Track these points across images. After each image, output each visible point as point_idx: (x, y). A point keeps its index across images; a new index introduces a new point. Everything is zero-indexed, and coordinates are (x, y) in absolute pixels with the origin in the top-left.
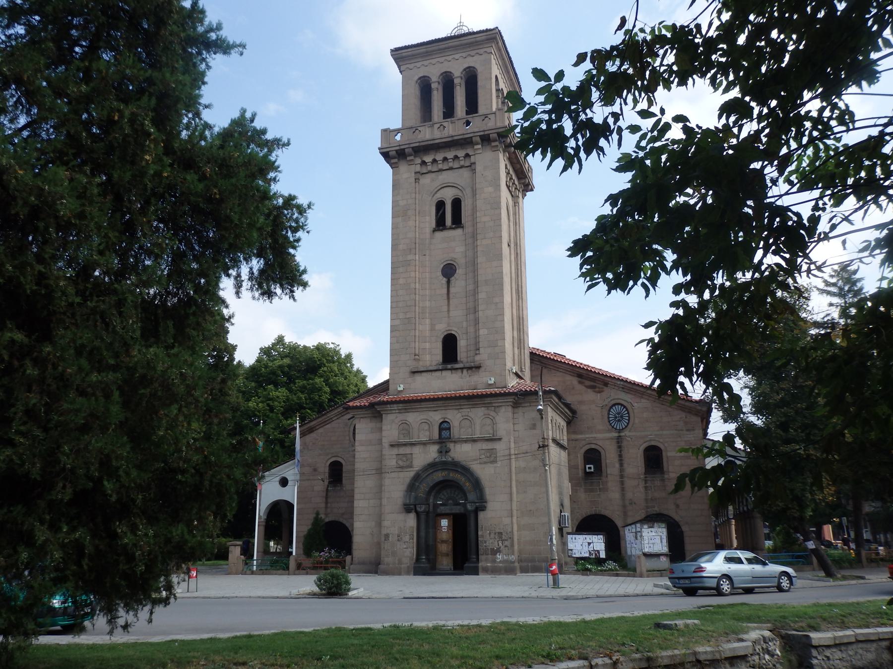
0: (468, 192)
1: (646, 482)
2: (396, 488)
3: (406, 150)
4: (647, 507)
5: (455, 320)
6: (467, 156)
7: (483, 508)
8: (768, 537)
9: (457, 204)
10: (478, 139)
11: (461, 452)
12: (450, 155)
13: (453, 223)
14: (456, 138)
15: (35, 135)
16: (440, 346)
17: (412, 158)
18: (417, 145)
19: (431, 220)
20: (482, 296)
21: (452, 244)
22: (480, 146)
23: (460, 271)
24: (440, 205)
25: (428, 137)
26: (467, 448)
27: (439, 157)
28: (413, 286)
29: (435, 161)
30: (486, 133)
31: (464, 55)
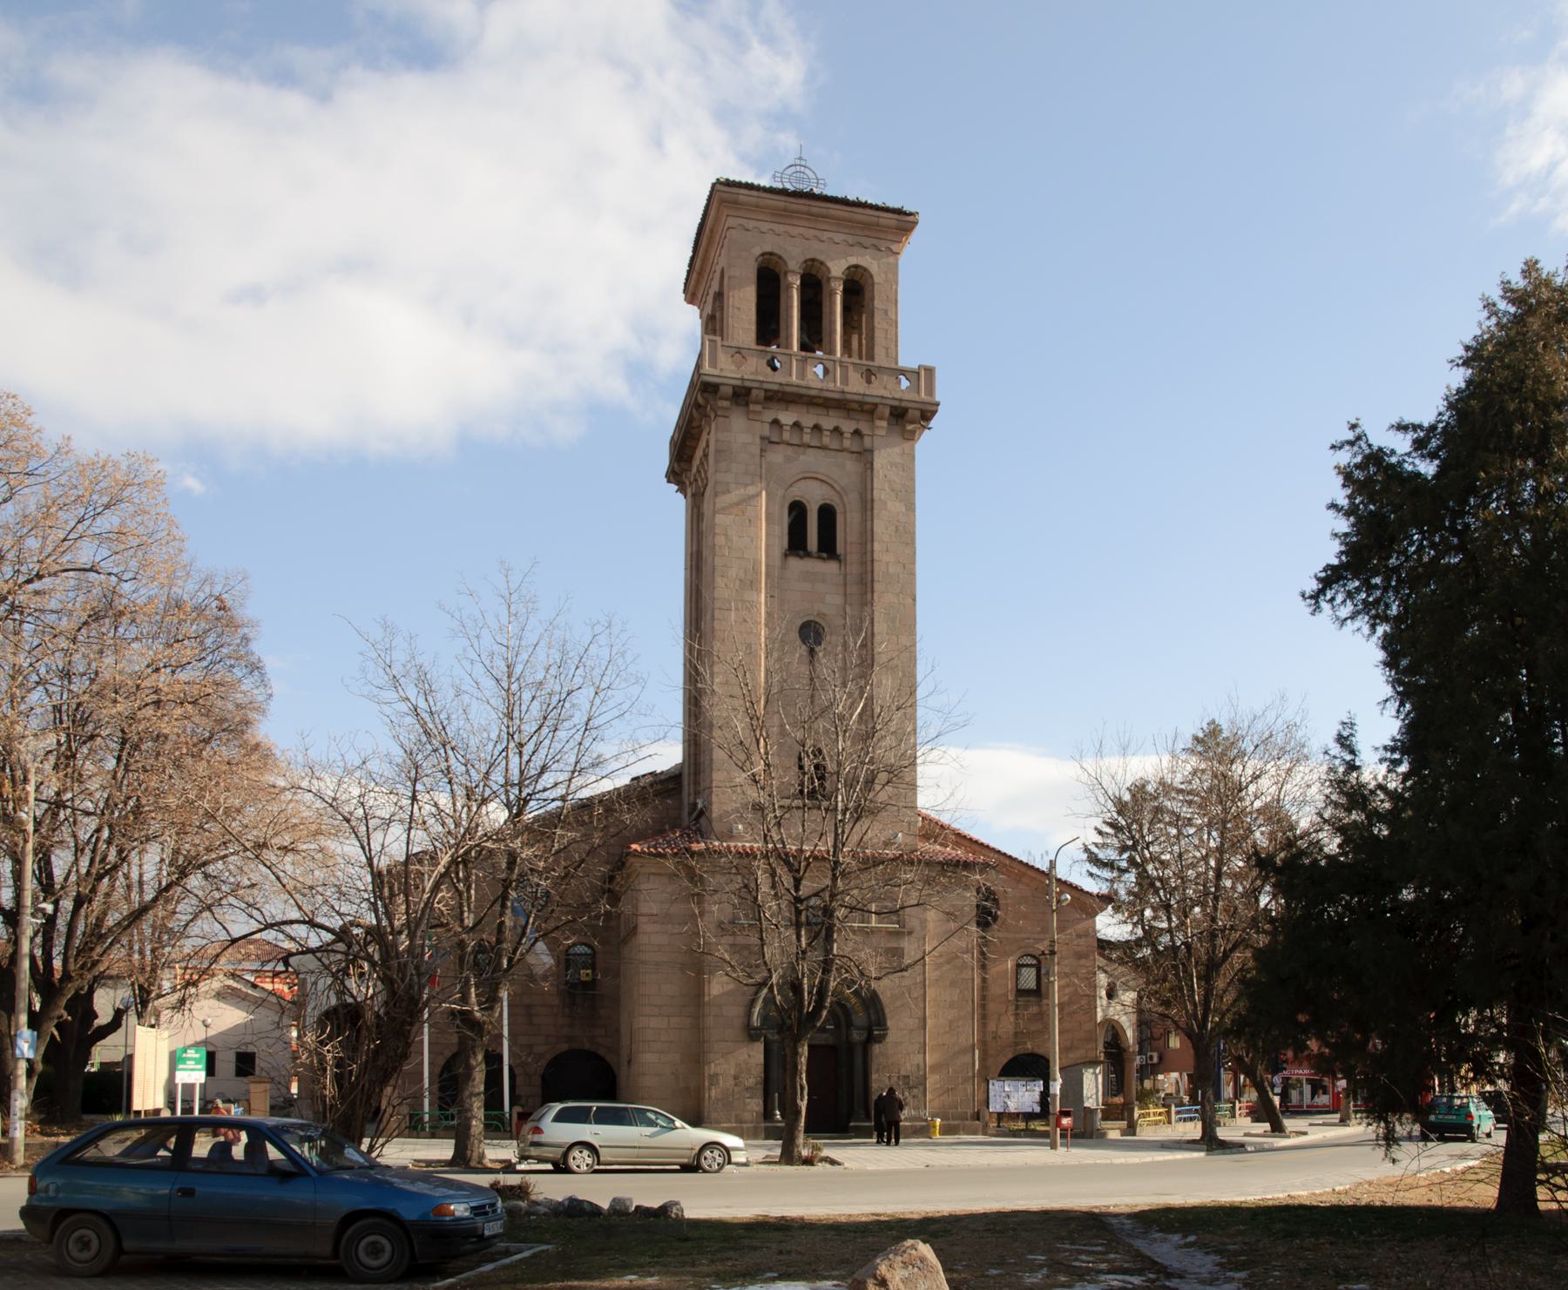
0: (852, 499)
3: (754, 392)
6: (857, 433)
7: (881, 1039)
8: (1360, 901)
9: (827, 515)
10: (887, 412)
12: (828, 422)
13: (820, 549)
15: (1420, 558)
17: (758, 408)
18: (775, 387)
22: (884, 424)
24: (797, 510)
30: (904, 404)
31: (851, 239)
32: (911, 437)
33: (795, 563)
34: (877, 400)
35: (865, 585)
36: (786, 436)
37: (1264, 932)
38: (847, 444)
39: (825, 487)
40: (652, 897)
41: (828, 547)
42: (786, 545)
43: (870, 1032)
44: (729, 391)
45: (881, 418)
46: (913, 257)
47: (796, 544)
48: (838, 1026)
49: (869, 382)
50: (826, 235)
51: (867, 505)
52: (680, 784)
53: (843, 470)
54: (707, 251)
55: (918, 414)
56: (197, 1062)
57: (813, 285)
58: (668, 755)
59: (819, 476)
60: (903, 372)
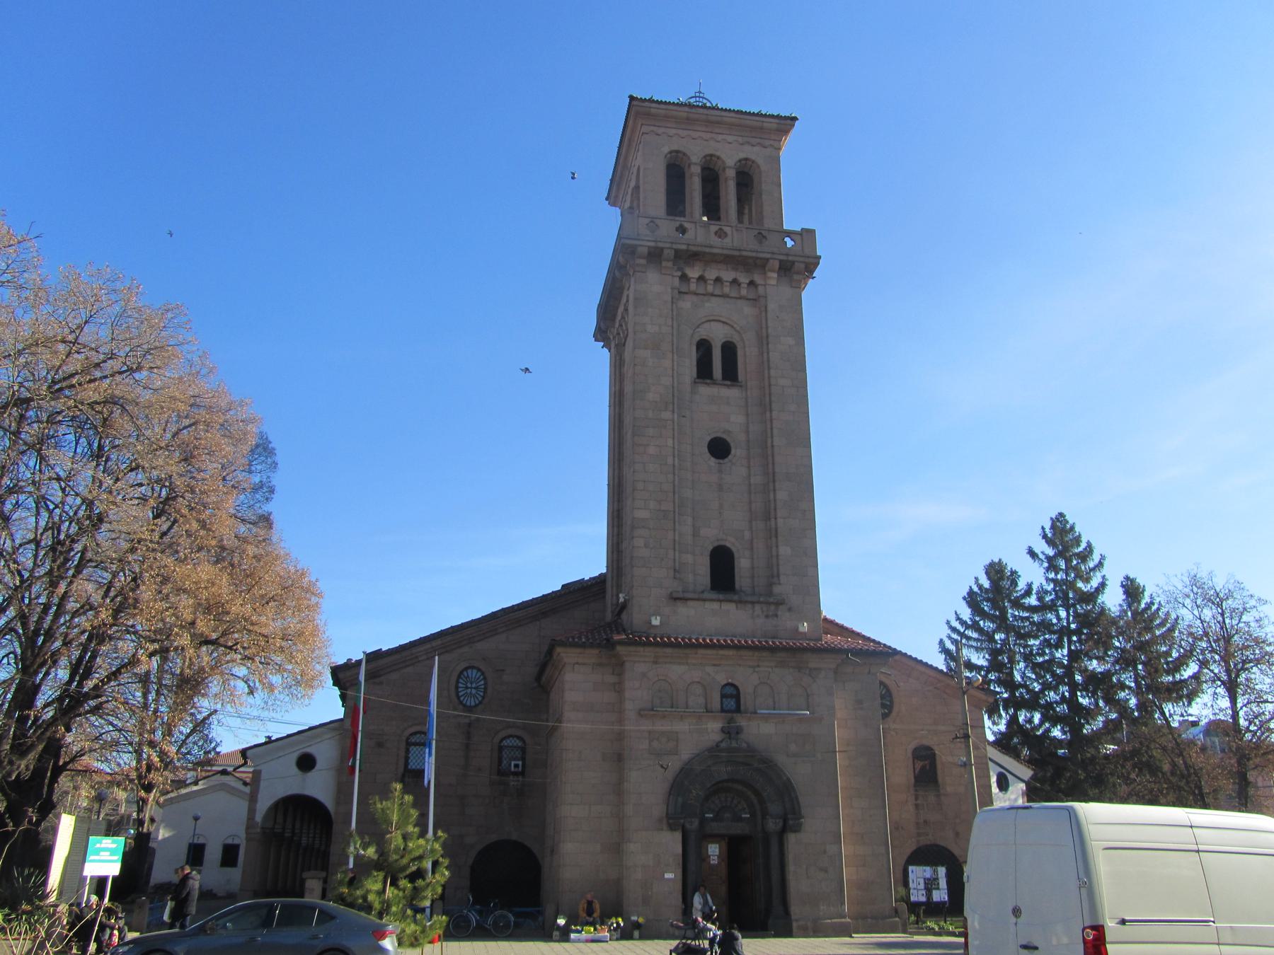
1: (916, 799)
2: (648, 786)
3: (666, 252)
4: (919, 835)
5: (729, 524)
7: (797, 829)
9: (729, 350)
10: (777, 265)
11: (760, 731)
12: (728, 275)
13: (724, 378)
14: (744, 253)
16: (706, 561)
18: (684, 247)
19: (689, 366)
20: (782, 495)
21: (722, 409)
22: (775, 275)
23: (737, 452)
24: (704, 347)
25: (700, 240)
26: (767, 729)
27: (711, 274)
28: (670, 461)
29: (701, 279)
32: (798, 287)
33: (705, 390)
34: (768, 256)
35: (765, 406)
36: (693, 286)
37: (1163, 713)
38: (744, 292)
39: (727, 327)
40: (578, 680)
41: (731, 374)
42: (695, 375)
43: (785, 821)
44: (645, 250)
45: (773, 271)
46: (791, 149)
47: (704, 371)
48: (753, 815)
49: (761, 242)
50: (720, 137)
51: (763, 340)
52: (603, 591)
53: (743, 314)
54: (626, 158)
55: (802, 266)
56: (113, 852)
57: (711, 177)
58: (593, 564)
59: (722, 318)
60: (789, 234)
